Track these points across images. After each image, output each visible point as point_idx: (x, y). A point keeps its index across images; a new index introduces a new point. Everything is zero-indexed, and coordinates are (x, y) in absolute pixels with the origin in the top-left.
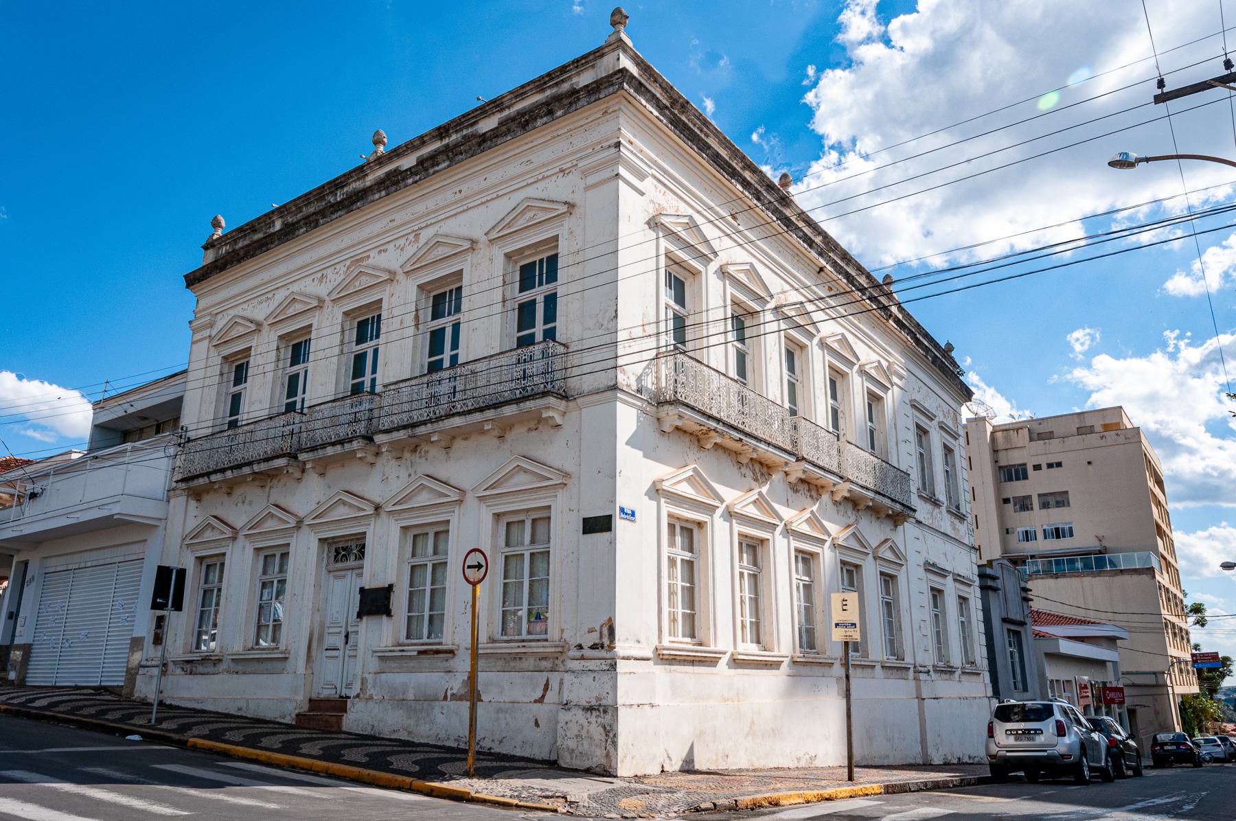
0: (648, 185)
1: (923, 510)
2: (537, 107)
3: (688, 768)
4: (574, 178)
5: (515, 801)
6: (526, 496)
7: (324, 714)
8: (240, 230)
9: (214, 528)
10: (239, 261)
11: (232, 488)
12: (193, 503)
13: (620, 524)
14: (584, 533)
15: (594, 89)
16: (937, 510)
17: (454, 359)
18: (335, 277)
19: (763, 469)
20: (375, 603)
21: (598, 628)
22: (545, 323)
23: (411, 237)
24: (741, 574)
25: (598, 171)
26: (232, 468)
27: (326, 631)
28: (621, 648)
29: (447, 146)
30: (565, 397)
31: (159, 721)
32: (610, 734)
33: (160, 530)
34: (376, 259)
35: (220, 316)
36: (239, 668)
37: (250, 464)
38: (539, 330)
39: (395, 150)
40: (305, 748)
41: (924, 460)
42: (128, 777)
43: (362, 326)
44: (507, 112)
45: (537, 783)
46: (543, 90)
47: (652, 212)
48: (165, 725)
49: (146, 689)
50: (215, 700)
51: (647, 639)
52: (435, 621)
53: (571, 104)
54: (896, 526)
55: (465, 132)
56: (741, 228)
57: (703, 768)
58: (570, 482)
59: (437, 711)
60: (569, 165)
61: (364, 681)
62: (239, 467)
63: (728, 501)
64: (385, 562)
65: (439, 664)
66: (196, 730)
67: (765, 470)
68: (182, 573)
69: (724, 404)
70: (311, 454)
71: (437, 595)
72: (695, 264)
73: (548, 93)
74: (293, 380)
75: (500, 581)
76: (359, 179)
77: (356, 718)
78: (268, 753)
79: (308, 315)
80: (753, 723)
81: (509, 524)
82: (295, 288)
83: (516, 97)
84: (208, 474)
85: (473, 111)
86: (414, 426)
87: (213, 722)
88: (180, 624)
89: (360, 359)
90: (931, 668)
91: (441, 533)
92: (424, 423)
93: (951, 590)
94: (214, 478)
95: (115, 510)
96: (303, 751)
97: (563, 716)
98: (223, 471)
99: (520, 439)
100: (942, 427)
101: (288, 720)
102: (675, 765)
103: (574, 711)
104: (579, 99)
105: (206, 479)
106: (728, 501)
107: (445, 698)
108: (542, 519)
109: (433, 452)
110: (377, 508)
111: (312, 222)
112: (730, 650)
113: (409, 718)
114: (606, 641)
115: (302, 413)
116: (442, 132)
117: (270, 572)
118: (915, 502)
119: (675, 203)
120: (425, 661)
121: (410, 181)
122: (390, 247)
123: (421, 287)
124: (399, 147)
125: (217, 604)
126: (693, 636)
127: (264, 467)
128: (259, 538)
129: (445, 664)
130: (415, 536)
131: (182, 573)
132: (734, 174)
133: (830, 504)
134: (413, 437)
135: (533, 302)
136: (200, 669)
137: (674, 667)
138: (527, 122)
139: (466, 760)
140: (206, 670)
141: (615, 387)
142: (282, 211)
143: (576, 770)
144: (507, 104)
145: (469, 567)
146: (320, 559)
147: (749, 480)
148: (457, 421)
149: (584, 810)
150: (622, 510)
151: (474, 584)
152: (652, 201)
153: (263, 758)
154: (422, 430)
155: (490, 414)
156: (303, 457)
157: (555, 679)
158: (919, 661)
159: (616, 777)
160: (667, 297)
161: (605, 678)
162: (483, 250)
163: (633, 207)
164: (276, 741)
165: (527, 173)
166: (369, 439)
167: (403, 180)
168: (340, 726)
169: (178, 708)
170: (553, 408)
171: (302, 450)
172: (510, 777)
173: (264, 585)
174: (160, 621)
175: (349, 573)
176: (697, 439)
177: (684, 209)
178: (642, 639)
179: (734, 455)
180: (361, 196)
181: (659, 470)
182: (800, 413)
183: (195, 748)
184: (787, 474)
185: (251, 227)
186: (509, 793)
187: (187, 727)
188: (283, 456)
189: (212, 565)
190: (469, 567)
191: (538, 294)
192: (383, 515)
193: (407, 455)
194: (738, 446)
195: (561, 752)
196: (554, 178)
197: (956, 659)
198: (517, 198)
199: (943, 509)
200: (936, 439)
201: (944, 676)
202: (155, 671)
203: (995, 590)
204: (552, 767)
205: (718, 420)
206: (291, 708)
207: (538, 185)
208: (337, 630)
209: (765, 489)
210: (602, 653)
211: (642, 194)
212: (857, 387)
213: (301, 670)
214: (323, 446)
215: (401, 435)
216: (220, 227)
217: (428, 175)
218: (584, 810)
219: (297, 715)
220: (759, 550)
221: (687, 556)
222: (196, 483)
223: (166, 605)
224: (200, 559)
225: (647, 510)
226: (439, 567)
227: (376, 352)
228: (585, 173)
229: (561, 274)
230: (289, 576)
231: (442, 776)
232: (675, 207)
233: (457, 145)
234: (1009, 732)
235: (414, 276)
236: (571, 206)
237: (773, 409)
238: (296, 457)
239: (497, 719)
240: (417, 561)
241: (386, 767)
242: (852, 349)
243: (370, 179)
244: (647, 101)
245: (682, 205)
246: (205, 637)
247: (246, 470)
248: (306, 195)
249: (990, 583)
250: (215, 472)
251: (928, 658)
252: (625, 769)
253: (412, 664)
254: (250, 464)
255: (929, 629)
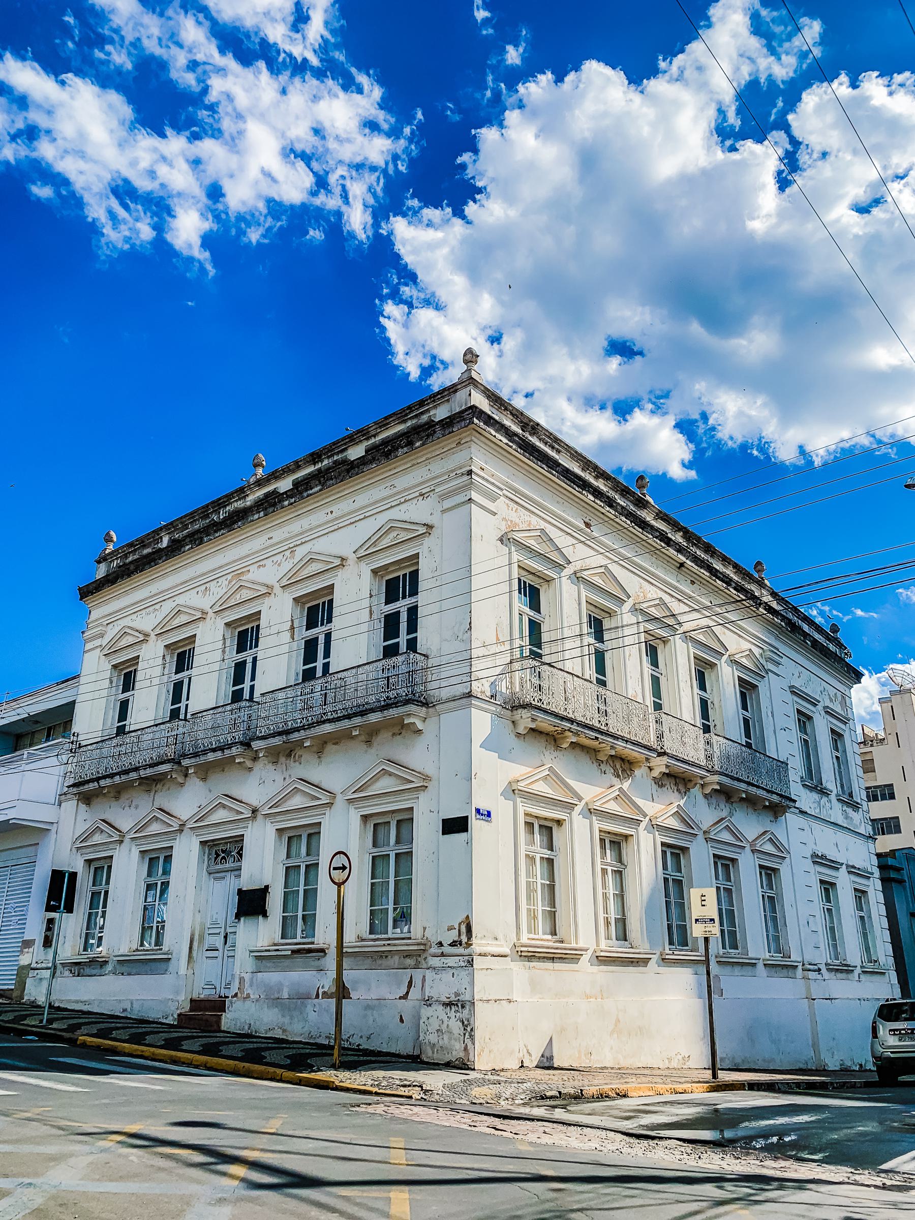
0: (501, 505)
1: (806, 799)
2: (399, 436)
3: (547, 1064)
4: (431, 501)
5: (375, 1090)
6: (392, 799)
7: (205, 1014)
8: (131, 545)
9: (102, 831)
10: (129, 576)
11: (119, 792)
12: (83, 807)
13: (475, 823)
14: (443, 834)
15: (449, 423)
16: (825, 799)
17: (326, 666)
18: (218, 590)
19: (623, 765)
20: (252, 904)
21: (457, 926)
22: (408, 634)
23: (287, 553)
24: (604, 871)
25: (453, 496)
26: (118, 774)
27: (207, 932)
28: (479, 944)
29: (319, 470)
30: (426, 704)
31: (50, 1021)
32: (468, 1028)
33: (53, 835)
34: (255, 574)
35: (111, 626)
36: (124, 969)
37: (136, 769)
38: (403, 639)
39: (273, 473)
40: (186, 1045)
41: (808, 748)
42: (33, 1066)
43: (243, 636)
44: (372, 441)
45: (397, 1074)
46: (405, 421)
47: (504, 529)
48: (54, 1026)
49: (36, 992)
50: (101, 1001)
51: (505, 936)
52: (309, 920)
53: (428, 436)
54: (776, 818)
55: (336, 458)
56: (595, 534)
57: (566, 1065)
58: (430, 785)
59: (309, 1008)
60: (428, 489)
61: (242, 980)
62: (126, 772)
63: (587, 798)
64: (263, 863)
65: (313, 963)
66: (84, 1030)
67: (626, 766)
68: (73, 875)
69: (581, 703)
70: (193, 760)
71: (311, 895)
72: (551, 573)
73: (409, 424)
74: (178, 686)
75: (367, 881)
76: (240, 499)
77: (231, 1020)
78: (152, 1049)
79: (192, 626)
80: (618, 1021)
81: (376, 826)
82: (180, 600)
83: (380, 427)
84: (98, 779)
85: (343, 439)
86: (287, 732)
87: (99, 1023)
88: (71, 926)
89: (240, 668)
90: (823, 968)
91: (314, 834)
92: (297, 730)
93: (845, 883)
94: (103, 783)
95: (11, 815)
96: (184, 1048)
97: (426, 1012)
98: (112, 776)
99: (387, 747)
100: (828, 712)
101: (170, 1021)
102: (531, 1062)
103: (434, 1007)
104: (435, 432)
105: (96, 784)
106: (587, 798)
107: (317, 996)
108: (405, 821)
109: (306, 756)
110: (254, 811)
111: (197, 539)
112: (592, 947)
113: (283, 1016)
114: (464, 939)
115: (185, 720)
116: (315, 457)
117: (154, 874)
118: (796, 790)
119: (528, 518)
120: (299, 960)
121: (286, 503)
122: (268, 562)
123: (296, 600)
124: (276, 471)
125: (105, 906)
126: (554, 933)
127: (149, 772)
128: (143, 841)
129: (317, 963)
130: (290, 838)
131: (73, 875)
132: (584, 485)
133: (700, 797)
134: (287, 745)
135: (398, 614)
136: (88, 971)
137: (532, 964)
138: (390, 452)
139: (333, 1055)
140: (94, 972)
141: (469, 695)
142: (170, 527)
143: (438, 1064)
144: (373, 433)
145: (335, 869)
146: (201, 861)
147: (610, 778)
148: (328, 728)
149: (437, 1097)
150: (478, 811)
151: (339, 885)
152: (504, 519)
153: (147, 1054)
154: (296, 736)
155: (357, 720)
156: (185, 762)
157: (418, 975)
158: (808, 958)
159: (474, 1069)
160: (520, 604)
161: (463, 973)
162: (352, 566)
163: (486, 526)
164: (159, 1039)
165: (391, 496)
166: (247, 745)
167: (280, 502)
168: (219, 1027)
169: (66, 1010)
170: (415, 716)
171: (184, 756)
172: (373, 1069)
173: (149, 887)
174: (51, 921)
175: (228, 874)
176: (553, 739)
177: (536, 523)
178: (500, 937)
179: (592, 752)
180: (241, 516)
181: (516, 770)
182: (665, 709)
183: (84, 1045)
184: (651, 769)
185: (142, 543)
186: (370, 1082)
187: (78, 1026)
188: (169, 761)
189: (101, 868)
190: (335, 869)
191: (402, 605)
192: (260, 817)
193: (282, 759)
194: (595, 744)
195: (424, 1047)
196: (415, 501)
197: (853, 954)
198: (382, 519)
199: (833, 797)
200: (822, 726)
201: (839, 975)
202: (47, 974)
203: (901, 882)
204: (415, 1061)
205: (571, 721)
206: (173, 1008)
207: (402, 507)
208: (217, 931)
209: (626, 785)
210: (460, 950)
211: (495, 514)
212: (726, 678)
213: (183, 970)
214: (205, 752)
215: (277, 741)
216: (112, 541)
217: (303, 498)
218: (437, 1097)
219: (179, 1015)
220: (623, 845)
221: (547, 853)
222: (87, 787)
223: (59, 907)
224: (89, 862)
225: (503, 810)
226: (312, 867)
227: (255, 660)
228: (443, 497)
229: (422, 586)
230: (173, 878)
231: (310, 1068)
232: (525, 521)
233: (328, 469)
234: (893, 1031)
235: (289, 590)
236: (430, 527)
237: (632, 705)
238: (179, 763)
239: (365, 1016)
240: (292, 862)
241: (260, 1060)
242: (719, 640)
243: (251, 499)
244: (496, 431)
245: (534, 519)
246: (91, 941)
247: (133, 775)
248: (191, 513)
249: (893, 875)
250: (104, 777)
251: (822, 957)
252: (482, 1061)
253: (287, 962)
254: (136, 769)
255: (819, 923)
